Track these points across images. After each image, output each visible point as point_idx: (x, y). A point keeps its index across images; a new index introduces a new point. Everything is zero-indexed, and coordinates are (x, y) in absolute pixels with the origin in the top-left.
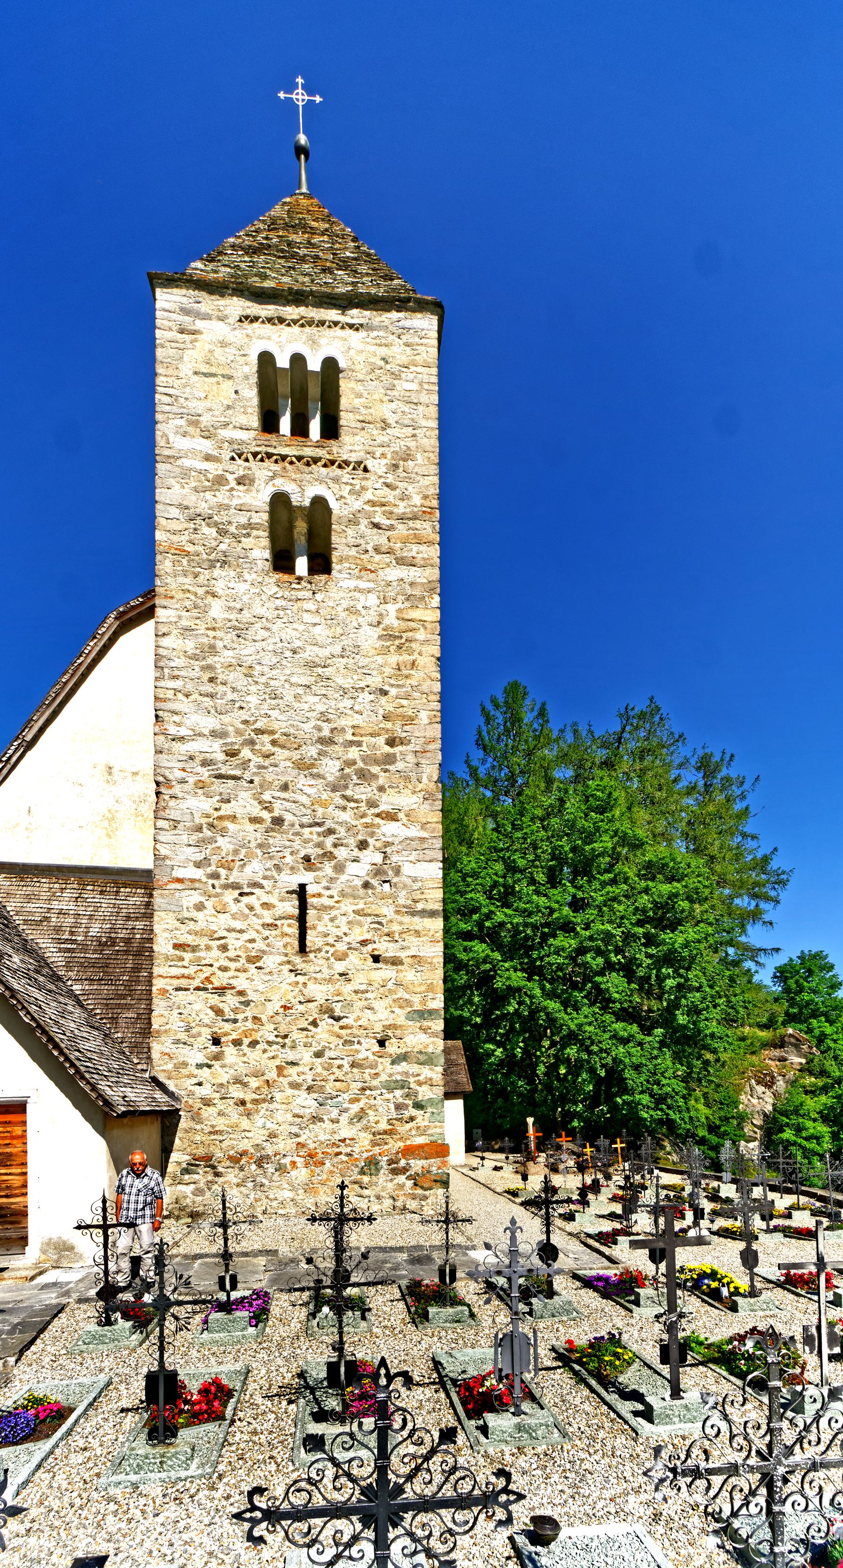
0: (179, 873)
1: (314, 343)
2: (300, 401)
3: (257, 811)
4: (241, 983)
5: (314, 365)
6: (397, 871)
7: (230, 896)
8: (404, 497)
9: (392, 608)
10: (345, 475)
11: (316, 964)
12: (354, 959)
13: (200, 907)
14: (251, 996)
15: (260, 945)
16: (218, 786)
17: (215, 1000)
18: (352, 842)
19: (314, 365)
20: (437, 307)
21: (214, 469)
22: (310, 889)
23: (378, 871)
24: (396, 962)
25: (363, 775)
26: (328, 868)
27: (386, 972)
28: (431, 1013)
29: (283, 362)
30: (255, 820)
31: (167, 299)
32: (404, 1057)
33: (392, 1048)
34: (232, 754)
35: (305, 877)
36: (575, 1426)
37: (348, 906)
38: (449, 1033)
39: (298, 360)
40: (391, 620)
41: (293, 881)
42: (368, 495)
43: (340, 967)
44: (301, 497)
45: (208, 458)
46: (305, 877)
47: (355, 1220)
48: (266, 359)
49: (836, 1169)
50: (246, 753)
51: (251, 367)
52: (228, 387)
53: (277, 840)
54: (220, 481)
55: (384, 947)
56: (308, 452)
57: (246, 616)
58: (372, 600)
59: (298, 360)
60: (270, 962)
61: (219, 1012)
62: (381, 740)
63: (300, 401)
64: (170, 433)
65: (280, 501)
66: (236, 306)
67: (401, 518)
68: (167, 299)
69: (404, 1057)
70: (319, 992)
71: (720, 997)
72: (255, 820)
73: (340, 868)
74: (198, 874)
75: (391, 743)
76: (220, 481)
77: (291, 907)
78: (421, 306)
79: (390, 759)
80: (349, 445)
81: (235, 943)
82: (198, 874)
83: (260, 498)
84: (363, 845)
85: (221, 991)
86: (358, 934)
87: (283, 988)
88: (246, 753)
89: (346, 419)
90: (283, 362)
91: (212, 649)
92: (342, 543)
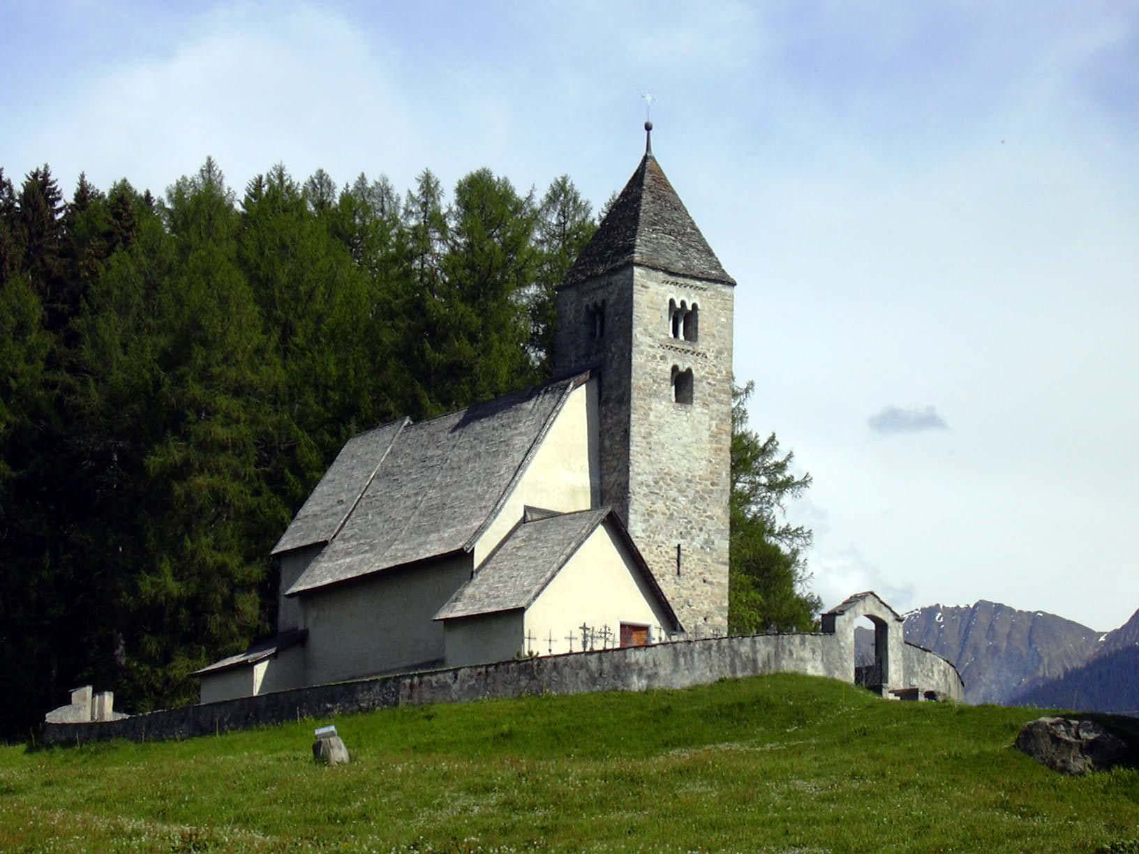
1: (689, 296)
3: (664, 509)
8: (720, 372)
9: (714, 423)
11: (683, 581)
12: (697, 580)
22: (682, 547)
23: (706, 542)
24: (711, 583)
25: (703, 498)
27: (708, 588)
28: (734, 672)
30: (664, 514)
34: (656, 483)
35: (681, 541)
37: (695, 557)
38: (730, 618)
40: (714, 428)
41: (675, 542)
44: (682, 368)
45: (651, 347)
47: (209, 172)
48: (672, 302)
49: (183, 768)
50: (661, 483)
51: (667, 306)
52: (658, 314)
53: (672, 524)
57: (662, 421)
58: (707, 418)
62: (708, 483)
64: (637, 331)
66: (661, 275)
72: (664, 514)
73: (693, 539)
74: (643, 535)
76: (654, 357)
77: (674, 554)
80: (701, 346)
84: (701, 530)
86: (699, 570)
91: (650, 434)
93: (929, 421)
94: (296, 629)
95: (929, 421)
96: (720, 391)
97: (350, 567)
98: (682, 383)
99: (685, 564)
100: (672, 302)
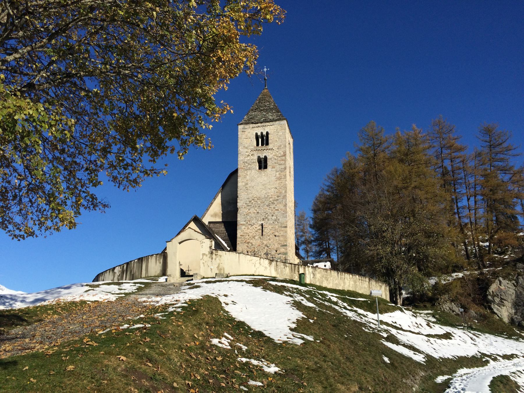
0: (242, 223)
2: (263, 140)
4: (251, 241)
5: (265, 133)
6: (279, 220)
7: (250, 226)
9: (278, 173)
10: (270, 151)
13: (245, 228)
14: (253, 244)
15: (255, 235)
16: (248, 207)
17: (247, 244)
18: (271, 215)
19: (265, 133)
20: (285, 119)
21: (247, 154)
24: (278, 236)
26: (266, 220)
29: (259, 134)
31: (240, 127)
32: (280, 254)
33: (278, 252)
36: (12, 106)
37: (270, 227)
39: (262, 133)
40: (278, 176)
41: (260, 223)
42: (274, 154)
43: (268, 238)
44: (262, 156)
46: (263, 222)
54: (249, 155)
55: (277, 234)
56: (258, 149)
59: (262, 133)
60: (256, 238)
61: (248, 247)
63: (263, 140)
64: (240, 149)
65: (259, 157)
67: (280, 157)
68: (240, 127)
69: (280, 254)
70: (265, 242)
71: (88, 152)
74: (244, 223)
75: (278, 197)
76: (249, 155)
77: (260, 227)
78: (284, 119)
79: (277, 200)
80: (270, 146)
81: (250, 235)
82: (244, 223)
83: (256, 158)
84: (273, 216)
85: (248, 243)
86: (271, 232)
87: (259, 242)
88: (253, 201)
89: (270, 141)
90: (259, 134)
92: (269, 163)
93: (180, 243)
94: (376, 281)
95: (180, 243)
96: (280, 161)
97: (290, 148)
98: (263, 164)
99: (265, 230)
100: (256, 134)
